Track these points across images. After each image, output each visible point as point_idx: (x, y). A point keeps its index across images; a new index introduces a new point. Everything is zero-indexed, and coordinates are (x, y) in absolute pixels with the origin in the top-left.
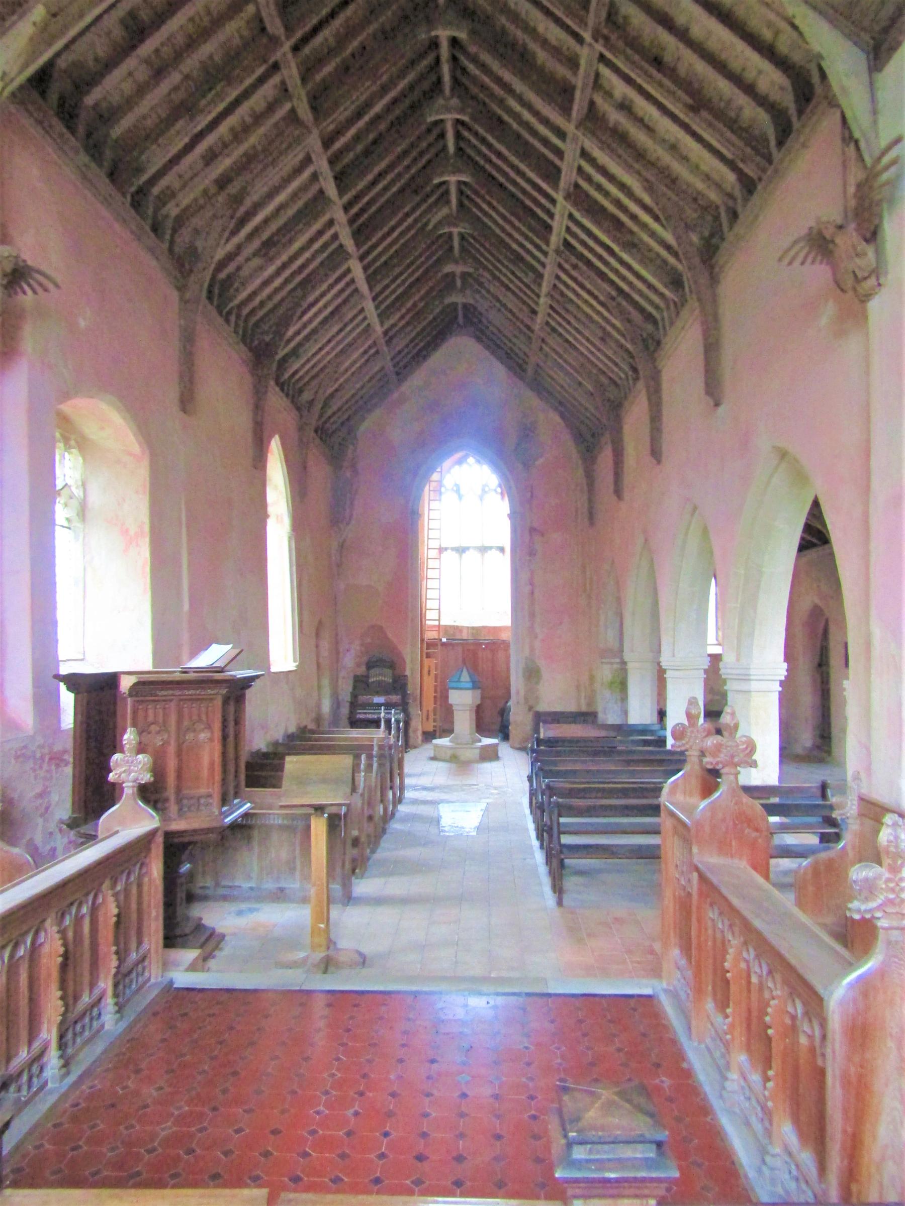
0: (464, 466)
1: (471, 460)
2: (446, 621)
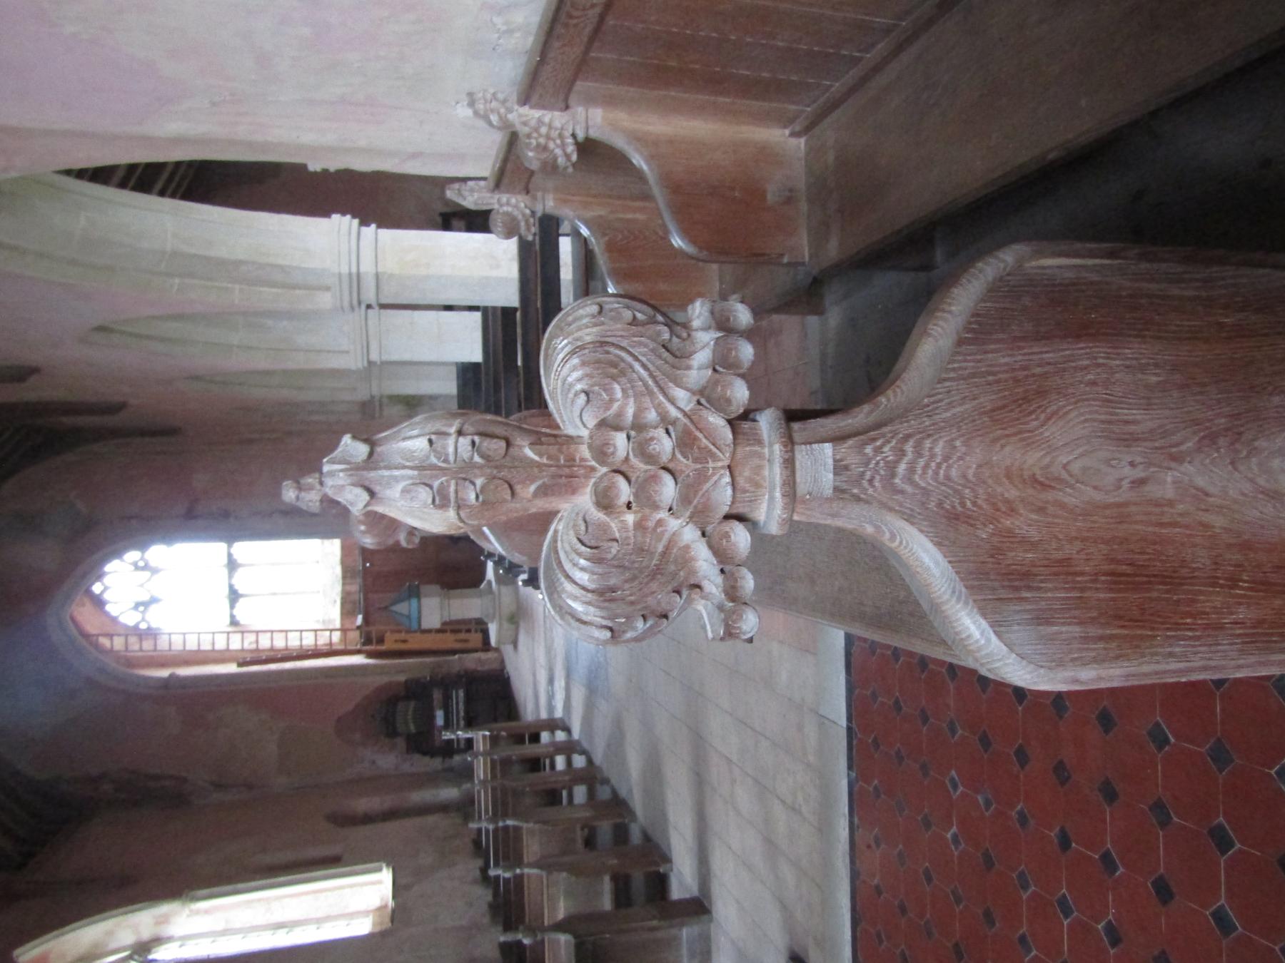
0: (106, 596)
1: (97, 588)
2: (334, 614)
